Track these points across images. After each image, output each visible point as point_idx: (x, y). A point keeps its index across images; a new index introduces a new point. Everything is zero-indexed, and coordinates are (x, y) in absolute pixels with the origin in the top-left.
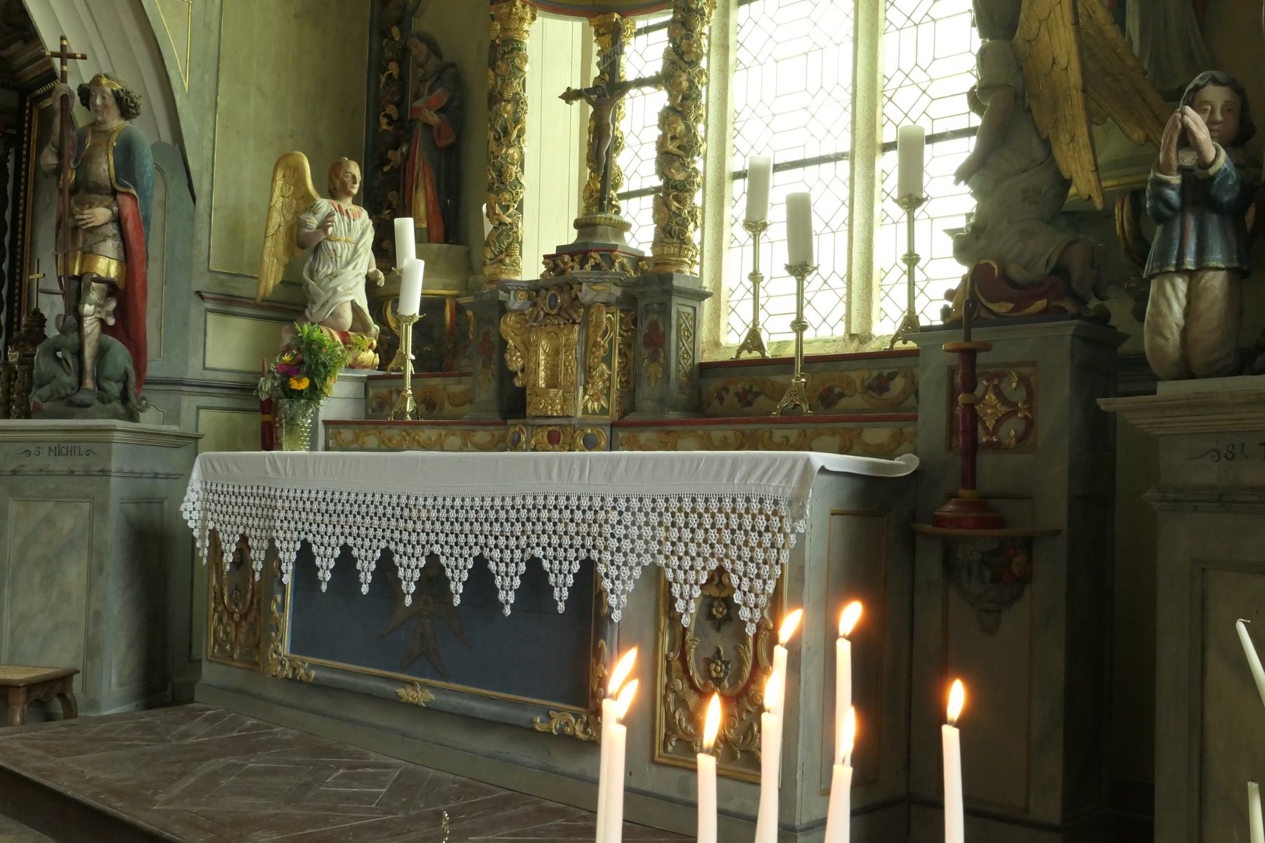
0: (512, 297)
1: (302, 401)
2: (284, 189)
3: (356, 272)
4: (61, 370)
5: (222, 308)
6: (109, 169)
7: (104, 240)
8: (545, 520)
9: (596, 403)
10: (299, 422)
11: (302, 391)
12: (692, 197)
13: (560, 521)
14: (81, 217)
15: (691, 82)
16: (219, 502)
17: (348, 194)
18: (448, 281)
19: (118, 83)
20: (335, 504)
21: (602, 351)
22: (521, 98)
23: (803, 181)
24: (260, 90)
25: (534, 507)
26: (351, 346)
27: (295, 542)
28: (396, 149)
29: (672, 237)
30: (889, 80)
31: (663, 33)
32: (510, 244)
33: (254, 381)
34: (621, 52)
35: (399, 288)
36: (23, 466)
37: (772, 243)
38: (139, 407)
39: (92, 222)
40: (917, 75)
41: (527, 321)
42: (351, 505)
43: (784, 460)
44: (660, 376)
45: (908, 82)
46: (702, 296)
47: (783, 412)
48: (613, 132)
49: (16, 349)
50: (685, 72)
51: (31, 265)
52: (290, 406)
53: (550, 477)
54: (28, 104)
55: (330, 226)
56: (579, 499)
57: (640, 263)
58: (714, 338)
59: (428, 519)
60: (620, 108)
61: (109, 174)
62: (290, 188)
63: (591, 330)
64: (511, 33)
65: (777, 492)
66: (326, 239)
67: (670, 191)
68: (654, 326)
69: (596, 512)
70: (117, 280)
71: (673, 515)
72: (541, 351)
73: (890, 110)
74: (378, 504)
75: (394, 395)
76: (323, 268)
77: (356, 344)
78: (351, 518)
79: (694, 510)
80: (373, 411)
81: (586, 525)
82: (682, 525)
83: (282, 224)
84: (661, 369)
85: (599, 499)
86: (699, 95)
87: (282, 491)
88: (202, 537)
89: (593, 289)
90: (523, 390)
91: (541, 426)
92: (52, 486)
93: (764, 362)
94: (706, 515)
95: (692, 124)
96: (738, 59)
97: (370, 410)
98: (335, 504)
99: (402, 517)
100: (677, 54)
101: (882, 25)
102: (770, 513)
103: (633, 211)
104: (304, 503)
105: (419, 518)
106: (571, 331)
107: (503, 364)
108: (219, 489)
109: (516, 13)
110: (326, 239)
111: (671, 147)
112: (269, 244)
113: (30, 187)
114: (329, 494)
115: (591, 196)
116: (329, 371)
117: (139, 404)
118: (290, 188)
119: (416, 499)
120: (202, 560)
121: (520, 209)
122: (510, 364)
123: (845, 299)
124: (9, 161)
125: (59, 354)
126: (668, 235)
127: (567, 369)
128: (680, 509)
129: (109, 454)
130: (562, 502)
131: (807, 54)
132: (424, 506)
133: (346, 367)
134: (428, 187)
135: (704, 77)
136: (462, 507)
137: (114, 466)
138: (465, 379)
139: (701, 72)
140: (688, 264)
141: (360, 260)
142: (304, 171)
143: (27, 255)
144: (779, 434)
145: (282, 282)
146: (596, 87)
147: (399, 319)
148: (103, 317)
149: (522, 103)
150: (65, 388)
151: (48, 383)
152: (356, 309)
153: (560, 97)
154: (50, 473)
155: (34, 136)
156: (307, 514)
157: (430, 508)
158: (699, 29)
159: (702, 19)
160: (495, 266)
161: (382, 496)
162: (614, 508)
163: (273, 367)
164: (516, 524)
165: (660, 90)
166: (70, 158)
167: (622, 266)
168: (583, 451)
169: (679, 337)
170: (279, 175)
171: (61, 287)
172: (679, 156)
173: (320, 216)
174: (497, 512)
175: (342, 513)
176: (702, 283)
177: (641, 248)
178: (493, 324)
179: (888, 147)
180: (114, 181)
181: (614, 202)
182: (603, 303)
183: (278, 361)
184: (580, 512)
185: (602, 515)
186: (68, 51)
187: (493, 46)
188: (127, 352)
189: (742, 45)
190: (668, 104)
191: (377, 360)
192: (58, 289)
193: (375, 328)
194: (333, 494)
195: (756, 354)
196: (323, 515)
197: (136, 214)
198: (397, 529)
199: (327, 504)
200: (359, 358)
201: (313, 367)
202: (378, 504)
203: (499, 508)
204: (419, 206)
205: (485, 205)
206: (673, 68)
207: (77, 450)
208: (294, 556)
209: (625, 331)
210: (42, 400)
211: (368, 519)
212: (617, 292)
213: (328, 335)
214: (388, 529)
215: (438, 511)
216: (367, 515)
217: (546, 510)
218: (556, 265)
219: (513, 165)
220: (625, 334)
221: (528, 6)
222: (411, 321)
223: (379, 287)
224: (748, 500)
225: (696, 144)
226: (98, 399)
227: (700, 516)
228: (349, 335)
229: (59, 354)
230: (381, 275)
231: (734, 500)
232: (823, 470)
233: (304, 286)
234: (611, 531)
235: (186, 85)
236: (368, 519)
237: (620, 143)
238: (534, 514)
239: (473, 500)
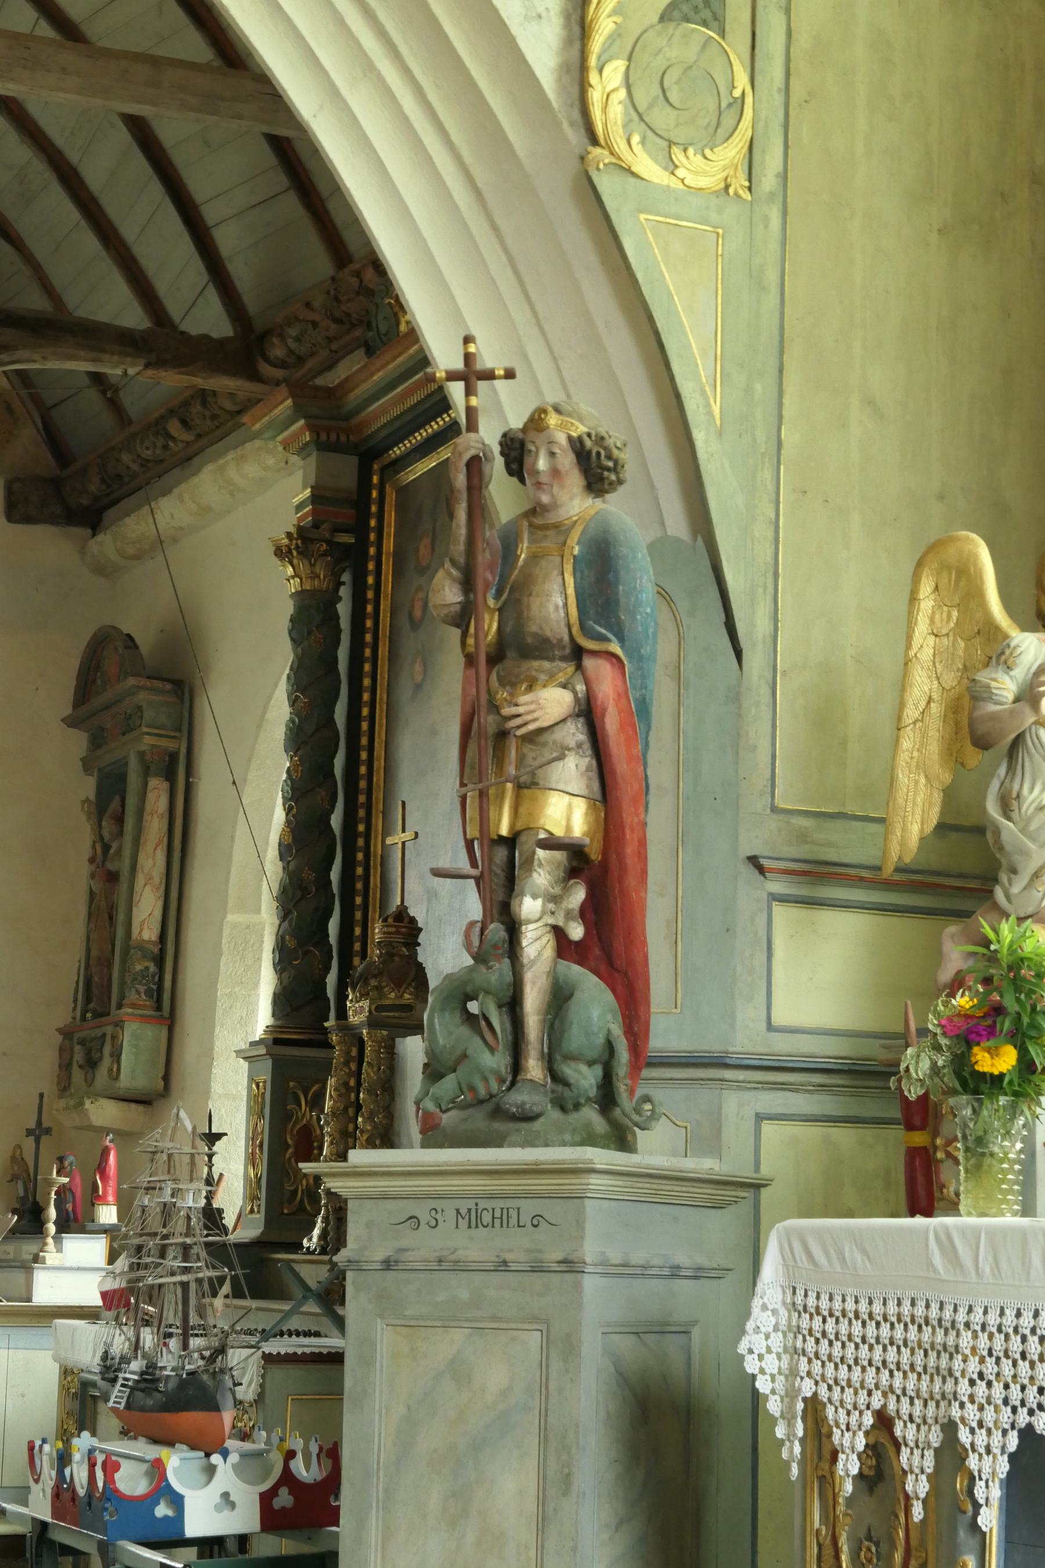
1: (1003, 1100)
2: (937, 617)
4: (477, 1041)
5: (804, 891)
6: (566, 605)
7: (561, 757)
11: (1002, 1076)
14: (513, 710)
16: (824, 1334)
19: (581, 420)
24: (869, 402)
27: (1005, 1432)
33: (890, 1056)
36: (407, 1250)
38: (636, 1117)
39: (535, 720)
49: (364, 995)
51: (386, 814)
52: (974, 1111)
54: (375, 479)
61: (567, 614)
62: (949, 616)
66: (1036, 723)
70: (587, 841)
76: (1032, 789)
83: (935, 696)
87: (970, 1310)
88: (788, 1416)
92: (464, 1295)
104: (1024, 1339)
108: (824, 1304)
110: (1036, 723)
112: (906, 744)
113: (383, 650)
117: (638, 1111)
118: (949, 616)
120: (789, 1469)
124: (340, 599)
125: (473, 1007)
129: (580, 1225)
137: (590, 1251)
142: (979, 574)
143: (378, 795)
148: (561, 924)
150: (485, 1079)
151: (454, 1071)
154: (459, 1267)
155: (389, 545)
166: (487, 586)
171: (474, 864)
180: (576, 629)
183: (941, 1008)
186: (479, 366)
188: (609, 996)
192: (463, 863)
197: (623, 695)
201: (1026, 1020)
207: (513, 1214)
208: (1003, 1467)
210: (440, 1107)
226: (551, 1101)
229: (473, 1007)
233: (989, 835)
235: (716, 410)
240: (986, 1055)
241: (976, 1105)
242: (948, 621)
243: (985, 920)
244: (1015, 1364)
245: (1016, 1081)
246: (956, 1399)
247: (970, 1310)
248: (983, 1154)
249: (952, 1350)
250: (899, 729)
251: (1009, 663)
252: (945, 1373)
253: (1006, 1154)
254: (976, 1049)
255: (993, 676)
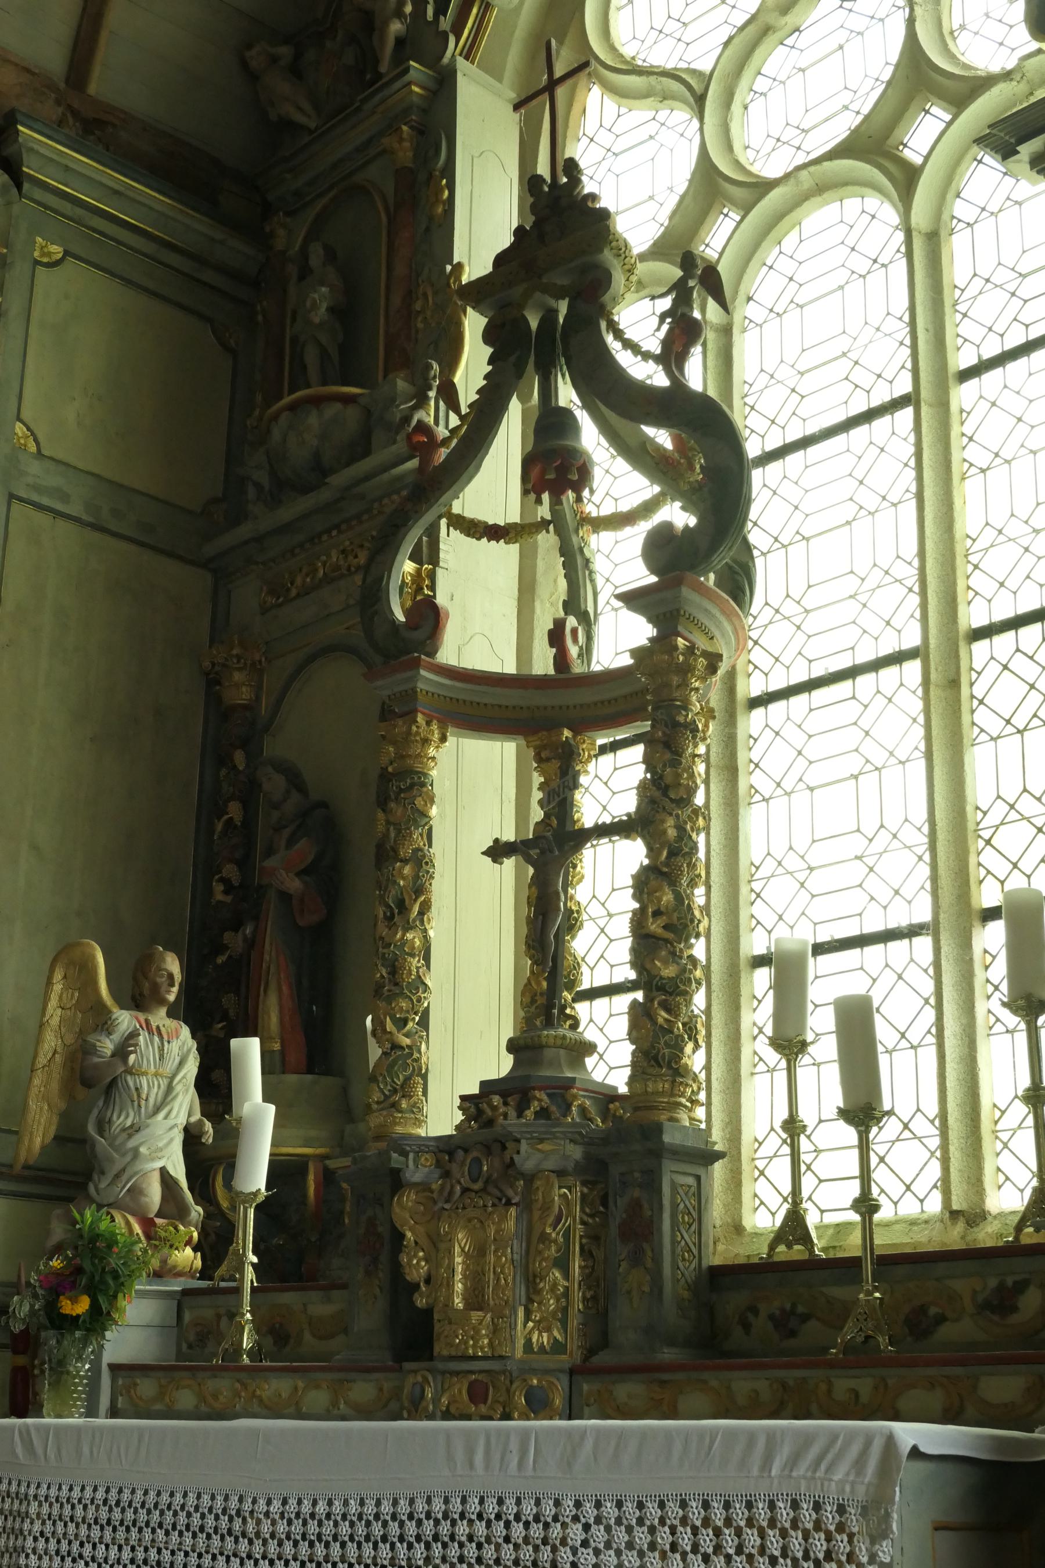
0: (411, 1163)
1: (78, 1334)
3: (170, 1122)
8: (464, 1539)
9: (545, 1335)
10: (71, 1369)
11: (78, 1316)
12: (689, 1002)
13: (488, 1540)
15: (681, 829)
17: (162, 1001)
18: (313, 1133)
20: (123, 1511)
21: (553, 1248)
22: (424, 856)
23: (862, 968)
25: (446, 1516)
26: (157, 1243)
28: (236, 930)
29: (661, 1067)
30: (985, 813)
31: (638, 751)
32: (408, 1079)
34: (576, 785)
35: (236, 1146)
37: (819, 1065)
40: (1014, 529)
41: (435, 1202)
42: (149, 1512)
43: (852, 1435)
44: (647, 1289)
45: (1013, 815)
46: (710, 1157)
47: (848, 1348)
48: (565, 904)
50: (671, 814)
52: (58, 1342)
53: (471, 1465)
55: (132, 1052)
56: (518, 1502)
57: (611, 1106)
58: (734, 1220)
59: (273, 1536)
60: (575, 867)
63: (536, 1214)
64: (409, 762)
65: (843, 1491)
67: (655, 993)
68: (636, 1206)
69: (546, 1526)
71: (673, 1531)
72: (457, 1249)
73: (989, 857)
74: (192, 1510)
75: (224, 1321)
76: (119, 1117)
77: (166, 1240)
78: (147, 1535)
79: (706, 1522)
80: (190, 1347)
81: (530, 1548)
82: (688, 1549)
83: (59, 1050)
84: (648, 1278)
85: (551, 1502)
86: (695, 848)
87: (38, 1486)
89: (539, 1150)
90: (428, 1312)
91: (457, 1373)
93: (814, 1264)
94: (727, 1532)
95: (685, 891)
96: (752, 786)
97: (184, 1346)
98: (123, 1511)
99: (230, 1532)
100: (659, 789)
101: (970, 734)
102: (832, 1528)
103: (600, 1019)
104: (73, 1507)
105: (258, 1535)
106: (504, 1218)
107: (396, 1270)
109: (418, 733)
111: (654, 927)
112: (36, 1081)
114: (114, 1492)
115: (533, 1001)
116: (122, 1284)
119: (254, 1501)
121: (424, 1023)
122: (407, 1270)
123: (938, 1154)
126: (653, 1062)
127: (498, 1279)
128: (684, 1521)
130: (491, 1508)
131: (856, 777)
132: (267, 1514)
133: (149, 1276)
134: (285, 988)
135: (701, 819)
136: (328, 1516)
138: (335, 1293)
139: (696, 811)
140: (686, 1107)
141: (176, 1104)
144: (842, 1385)
145: (56, 1138)
146: (537, 838)
147: (238, 1198)
149: (427, 863)
152: (167, 1180)
153: (483, 853)
156: (77, 1526)
157: (277, 1517)
158: (690, 750)
159: (694, 737)
160: (385, 1113)
161: (199, 1497)
162: (576, 1519)
163: (34, 1278)
164: (416, 1545)
165: (634, 840)
167: (583, 1110)
168: (528, 1419)
169: (675, 1225)
170: (58, 976)
172: (667, 941)
173: (116, 1037)
174: (385, 1524)
175: (134, 1525)
176: (710, 1136)
177: (625, 879)
178: (382, 1205)
179: (990, 914)
181: (568, 1011)
182: (553, 1172)
184: (521, 1525)
185: (556, 1531)
187: (384, 777)
189: (757, 765)
190: (646, 862)
191: (198, 1263)
193: (197, 1211)
194: (120, 1491)
195: (798, 1252)
196: (102, 1528)
198: (222, 1554)
199: (111, 1510)
200: (169, 1262)
201: (97, 1278)
202: (192, 1510)
203: (388, 1518)
204: (269, 1017)
205: (369, 1018)
206: (653, 809)
209: (591, 1216)
211: (174, 1536)
212: (576, 1152)
213: (123, 1225)
214: (207, 1552)
215: (290, 1522)
216: (174, 1528)
217: (465, 1522)
218: (480, 1112)
219: (413, 956)
220: (590, 1221)
221: (435, 722)
222: (254, 1200)
223: (204, 1144)
224: (795, 1505)
225: (692, 921)
227: (718, 1533)
228: (154, 1224)
230: (208, 1126)
231: (772, 1506)
232: (915, 1453)
234: (571, 1558)
236: (174, 1536)
237: (577, 920)
238: (445, 1528)
239: (346, 1503)
240: (68, 1302)
241: (59, 1337)
242: (72, 999)
243: (76, 1209)
244: (65, 1525)
245: (88, 1320)
246: (23, 1551)
247: (38, 1486)
248: (62, 1373)
249: (24, 1515)
250: (32, 1071)
251: (110, 1030)
252: (18, 1532)
253: (78, 1372)
254: (61, 1298)
255: (99, 1038)
